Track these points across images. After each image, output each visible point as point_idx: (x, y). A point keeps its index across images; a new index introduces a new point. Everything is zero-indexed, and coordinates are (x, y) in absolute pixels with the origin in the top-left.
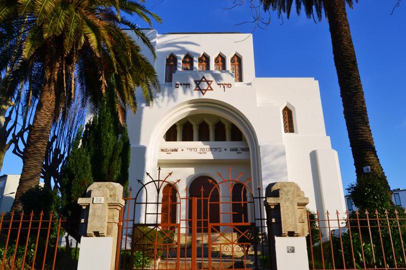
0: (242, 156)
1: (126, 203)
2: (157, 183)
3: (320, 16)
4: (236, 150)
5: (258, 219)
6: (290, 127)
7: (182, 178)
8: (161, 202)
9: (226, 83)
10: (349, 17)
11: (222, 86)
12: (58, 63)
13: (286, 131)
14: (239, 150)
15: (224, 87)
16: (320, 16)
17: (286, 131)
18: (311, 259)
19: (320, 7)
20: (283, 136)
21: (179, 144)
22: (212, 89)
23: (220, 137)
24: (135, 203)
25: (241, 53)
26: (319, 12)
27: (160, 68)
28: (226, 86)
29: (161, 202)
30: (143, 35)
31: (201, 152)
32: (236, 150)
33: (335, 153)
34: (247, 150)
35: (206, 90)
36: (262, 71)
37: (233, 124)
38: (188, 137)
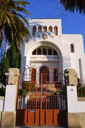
0: (57, 60)
4: (55, 58)
6: (72, 50)
7: (38, 66)
13: (71, 52)
17: (71, 52)
22: (47, 38)
23: (50, 53)
25: (57, 26)
27: (31, 31)
30: (25, 19)
32: (55, 58)
34: (59, 58)
38: (39, 53)
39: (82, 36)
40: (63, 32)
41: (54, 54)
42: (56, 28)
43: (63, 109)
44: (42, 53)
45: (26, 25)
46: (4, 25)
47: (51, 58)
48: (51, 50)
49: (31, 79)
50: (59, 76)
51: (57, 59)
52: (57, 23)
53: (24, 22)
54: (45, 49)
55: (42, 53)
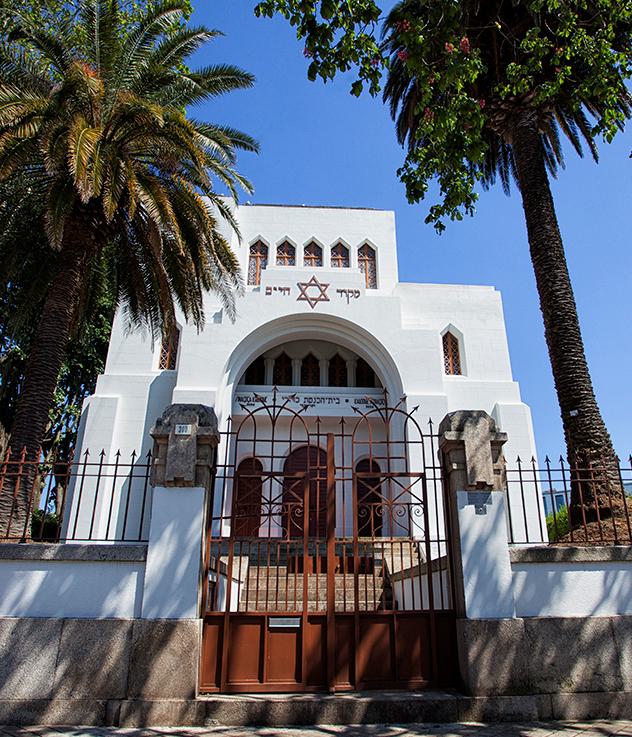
1: (406, 422)
2: (271, 410)
3: (506, 186)
5: (225, 518)
7: (273, 453)
8: (444, 539)
9: (351, 289)
10: (551, 187)
11: (344, 294)
12: (78, 286)
13: (448, 372)
15: (347, 296)
16: (506, 186)
17: (448, 372)
18: (299, 558)
19: (507, 172)
20: (444, 380)
21: (266, 391)
24: (237, 440)
25: (374, 242)
26: (505, 178)
27: (241, 253)
28: (350, 294)
29: (444, 539)
30: (221, 202)
31: (307, 403)
33: (528, 409)
35: (316, 300)
36: (409, 272)
37: (361, 359)
38: (283, 378)
39: (499, 293)
40: (405, 276)
41: (359, 384)
42: (368, 252)
43: (224, 610)
44: (324, 375)
45: (223, 228)
46: (133, 222)
47: (343, 401)
48: (344, 362)
49: (82, 461)
50: (339, 485)
52: (377, 227)
53: (216, 214)
54: (337, 355)
55: (324, 375)
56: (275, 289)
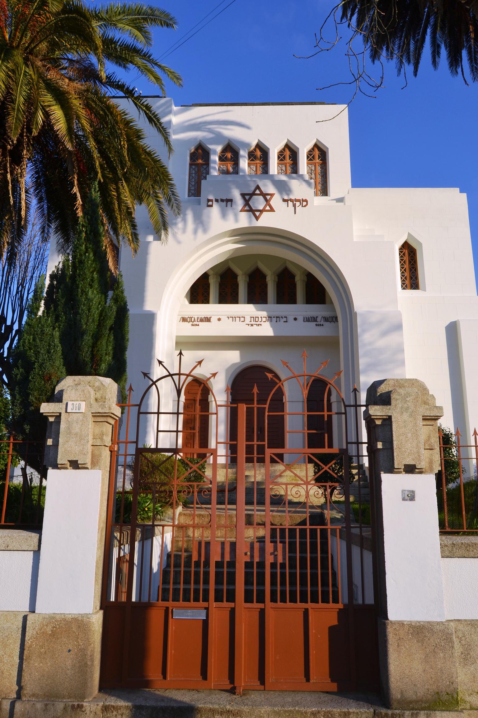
14: (319, 319)
51: (327, 324)
56: (282, 317)
